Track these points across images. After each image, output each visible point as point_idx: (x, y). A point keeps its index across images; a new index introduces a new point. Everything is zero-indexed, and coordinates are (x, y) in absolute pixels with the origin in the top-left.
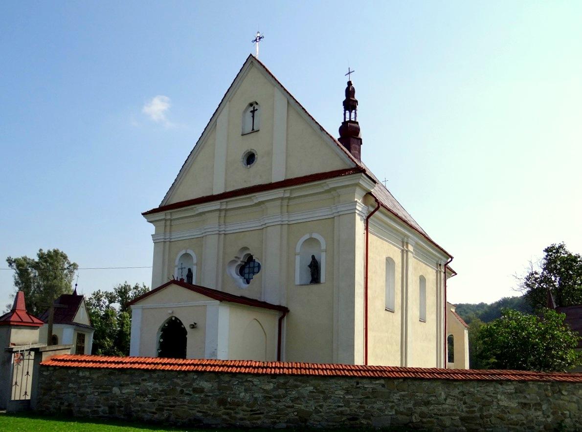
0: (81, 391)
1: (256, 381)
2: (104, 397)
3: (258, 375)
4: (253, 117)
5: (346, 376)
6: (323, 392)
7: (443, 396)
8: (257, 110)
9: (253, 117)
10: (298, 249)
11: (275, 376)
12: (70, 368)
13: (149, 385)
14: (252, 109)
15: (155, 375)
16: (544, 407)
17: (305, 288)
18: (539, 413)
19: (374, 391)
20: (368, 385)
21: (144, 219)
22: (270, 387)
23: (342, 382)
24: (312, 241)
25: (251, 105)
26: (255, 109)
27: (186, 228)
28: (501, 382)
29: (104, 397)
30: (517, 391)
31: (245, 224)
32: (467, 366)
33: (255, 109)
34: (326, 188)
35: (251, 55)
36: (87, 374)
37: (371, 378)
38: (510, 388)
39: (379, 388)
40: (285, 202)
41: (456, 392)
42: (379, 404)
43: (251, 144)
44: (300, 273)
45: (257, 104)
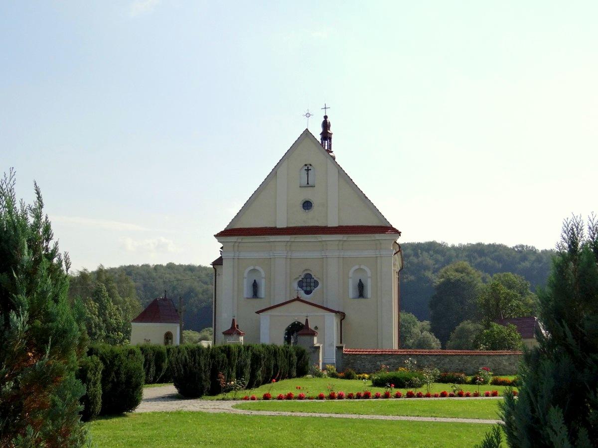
0: (363, 364)
1: (430, 358)
2: (373, 366)
3: (431, 355)
4: (308, 174)
5: (453, 355)
6: (452, 361)
7: (487, 361)
8: (310, 170)
9: (308, 174)
10: (351, 274)
11: (436, 355)
12: (357, 354)
13: (392, 360)
14: (307, 169)
15: (393, 356)
16: (516, 365)
17: (356, 300)
18: (514, 367)
19: (467, 360)
20: (465, 358)
21: (216, 240)
22: (435, 360)
23: (457, 357)
24: (360, 270)
25: (306, 165)
26: (309, 169)
27: (253, 248)
28: (504, 355)
29: (373, 366)
30: (509, 359)
31: (307, 252)
32: (395, 346)
33: (309, 169)
34: (373, 239)
35: (307, 129)
36: (365, 357)
37: (466, 355)
38: (506, 358)
39: (469, 359)
40: (341, 243)
41: (490, 360)
42: (469, 365)
43: (307, 195)
44: (352, 291)
45: (311, 165)
